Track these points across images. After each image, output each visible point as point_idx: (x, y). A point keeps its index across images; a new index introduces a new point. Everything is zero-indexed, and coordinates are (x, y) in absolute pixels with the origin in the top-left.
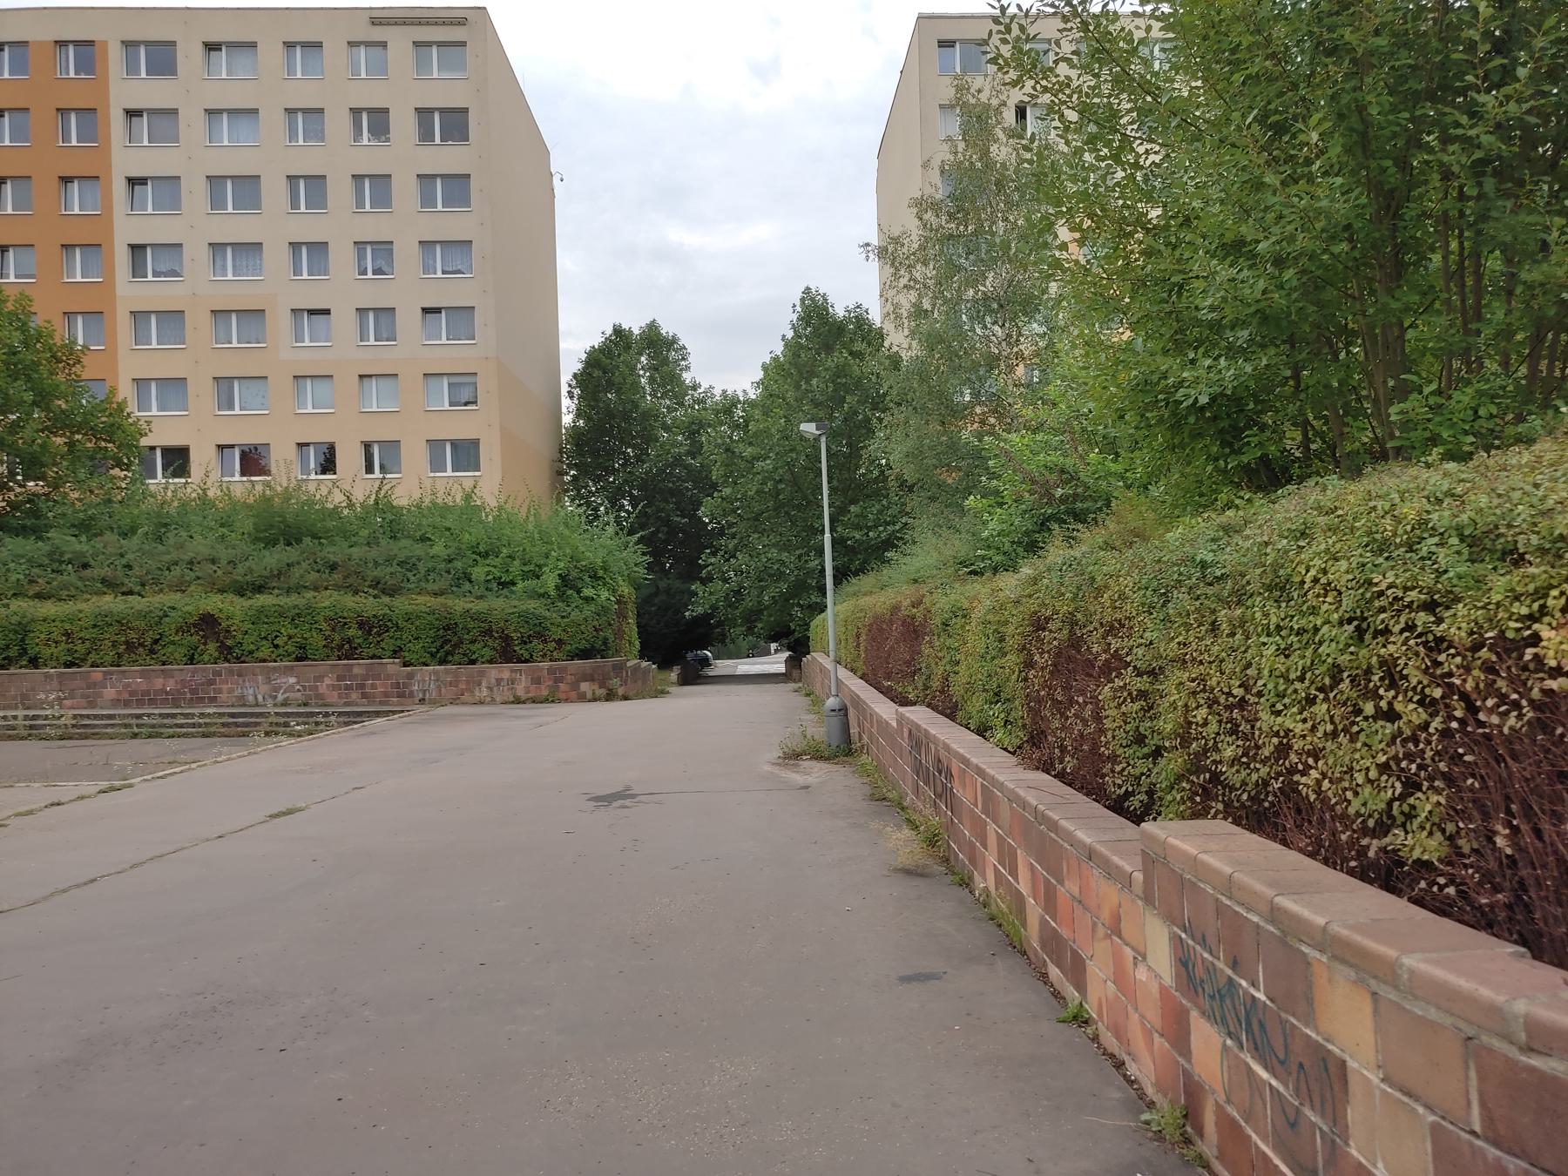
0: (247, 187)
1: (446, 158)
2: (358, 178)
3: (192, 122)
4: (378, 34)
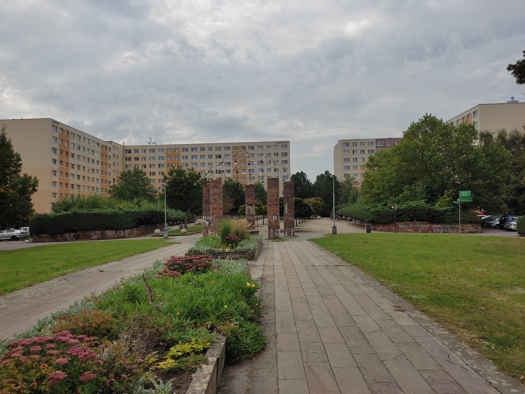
1: (285, 158)
4: (277, 144)
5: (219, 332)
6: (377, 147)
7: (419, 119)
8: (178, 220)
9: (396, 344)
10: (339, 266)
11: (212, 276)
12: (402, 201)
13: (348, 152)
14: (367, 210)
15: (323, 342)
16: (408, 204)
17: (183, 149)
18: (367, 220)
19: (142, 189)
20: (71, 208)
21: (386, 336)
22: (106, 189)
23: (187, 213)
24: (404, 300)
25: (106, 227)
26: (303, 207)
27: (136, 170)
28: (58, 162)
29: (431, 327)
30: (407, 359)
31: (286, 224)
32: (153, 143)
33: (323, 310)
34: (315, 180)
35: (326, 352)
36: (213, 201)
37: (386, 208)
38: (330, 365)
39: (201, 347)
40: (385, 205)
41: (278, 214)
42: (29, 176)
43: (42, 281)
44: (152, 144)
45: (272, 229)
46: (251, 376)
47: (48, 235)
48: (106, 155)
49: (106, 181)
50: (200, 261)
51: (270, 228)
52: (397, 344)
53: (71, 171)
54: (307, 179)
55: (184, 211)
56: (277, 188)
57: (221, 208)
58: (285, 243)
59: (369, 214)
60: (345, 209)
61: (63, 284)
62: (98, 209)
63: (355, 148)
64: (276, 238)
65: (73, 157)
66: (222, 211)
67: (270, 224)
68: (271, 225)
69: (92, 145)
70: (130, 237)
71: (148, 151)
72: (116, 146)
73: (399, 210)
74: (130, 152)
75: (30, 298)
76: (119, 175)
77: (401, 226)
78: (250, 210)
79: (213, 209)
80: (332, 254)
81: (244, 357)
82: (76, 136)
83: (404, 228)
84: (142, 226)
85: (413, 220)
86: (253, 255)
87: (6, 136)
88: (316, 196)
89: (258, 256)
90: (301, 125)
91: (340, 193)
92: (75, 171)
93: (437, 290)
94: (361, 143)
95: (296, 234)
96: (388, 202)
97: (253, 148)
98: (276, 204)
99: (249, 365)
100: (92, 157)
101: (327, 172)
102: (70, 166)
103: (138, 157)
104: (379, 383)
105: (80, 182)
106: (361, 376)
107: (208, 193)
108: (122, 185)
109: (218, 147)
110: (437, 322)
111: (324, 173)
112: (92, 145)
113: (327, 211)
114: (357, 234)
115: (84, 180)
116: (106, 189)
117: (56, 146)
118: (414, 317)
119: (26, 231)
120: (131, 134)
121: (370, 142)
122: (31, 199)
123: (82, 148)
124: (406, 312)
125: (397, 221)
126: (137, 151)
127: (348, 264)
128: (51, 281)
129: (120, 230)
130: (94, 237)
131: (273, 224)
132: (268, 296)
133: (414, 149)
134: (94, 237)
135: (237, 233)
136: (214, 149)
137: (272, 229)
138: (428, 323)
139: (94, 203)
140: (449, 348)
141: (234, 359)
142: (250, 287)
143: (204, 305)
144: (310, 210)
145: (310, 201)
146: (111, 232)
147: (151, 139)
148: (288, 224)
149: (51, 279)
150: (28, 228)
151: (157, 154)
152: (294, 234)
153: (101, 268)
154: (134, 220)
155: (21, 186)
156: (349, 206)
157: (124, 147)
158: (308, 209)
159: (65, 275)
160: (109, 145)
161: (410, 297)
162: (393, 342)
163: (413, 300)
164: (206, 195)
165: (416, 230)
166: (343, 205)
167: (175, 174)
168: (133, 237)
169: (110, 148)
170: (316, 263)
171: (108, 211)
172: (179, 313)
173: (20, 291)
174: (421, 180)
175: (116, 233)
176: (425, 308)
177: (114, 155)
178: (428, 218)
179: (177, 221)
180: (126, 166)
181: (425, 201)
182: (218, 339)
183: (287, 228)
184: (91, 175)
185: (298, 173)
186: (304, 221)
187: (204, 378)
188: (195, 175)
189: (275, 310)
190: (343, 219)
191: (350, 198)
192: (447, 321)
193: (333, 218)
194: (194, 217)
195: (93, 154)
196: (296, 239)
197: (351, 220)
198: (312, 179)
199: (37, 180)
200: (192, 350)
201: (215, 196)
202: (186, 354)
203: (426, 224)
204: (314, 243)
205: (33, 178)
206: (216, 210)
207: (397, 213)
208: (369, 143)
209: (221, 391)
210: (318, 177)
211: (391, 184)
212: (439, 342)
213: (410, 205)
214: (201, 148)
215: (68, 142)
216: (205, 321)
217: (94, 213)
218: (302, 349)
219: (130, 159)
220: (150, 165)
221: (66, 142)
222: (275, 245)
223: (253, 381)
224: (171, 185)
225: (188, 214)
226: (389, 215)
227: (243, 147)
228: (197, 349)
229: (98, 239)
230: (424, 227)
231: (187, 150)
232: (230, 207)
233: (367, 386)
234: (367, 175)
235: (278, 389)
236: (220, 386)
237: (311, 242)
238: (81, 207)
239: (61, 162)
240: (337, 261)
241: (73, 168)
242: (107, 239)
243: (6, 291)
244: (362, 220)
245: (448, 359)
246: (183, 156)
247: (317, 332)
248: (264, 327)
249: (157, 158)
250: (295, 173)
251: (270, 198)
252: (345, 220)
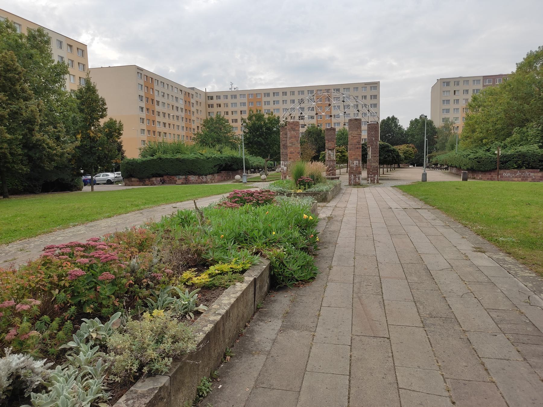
1: (374, 101)
5: (262, 256)
6: (484, 86)
7: (539, 47)
8: (259, 167)
9: (465, 282)
10: (420, 209)
11: (270, 208)
12: (509, 145)
14: (465, 157)
15: (381, 276)
16: (516, 149)
17: (265, 94)
18: (465, 168)
19: (225, 137)
20: (156, 153)
21: (456, 275)
22: (190, 137)
23: (266, 159)
24: (488, 242)
25: (189, 172)
26: (391, 152)
27: (218, 117)
28: (145, 109)
29: (514, 268)
30: (475, 297)
31: (370, 170)
32: (235, 89)
33: (389, 248)
34: (408, 126)
35: (381, 285)
36: (290, 145)
37: (488, 154)
38: (383, 297)
39: (240, 267)
40: (488, 150)
41: (360, 158)
42: (114, 120)
43: (120, 214)
44: (233, 90)
45: (352, 175)
46: (294, 301)
47: (137, 180)
48: (189, 102)
49: (190, 128)
50: (261, 195)
51: (350, 174)
52: (467, 283)
53: (158, 119)
54: (398, 124)
55: (264, 158)
56: (359, 130)
57: (298, 151)
58: (366, 189)
59: (468, 161)
60: (441, 157)
61: (137, 217)
62: (181, 155)
63: (456, 88)
64: (357, 185)
65: (158, 105)
66: (299, 155)
67: (351, 169)
68: (352, 171)
69: (175, 92)
70: (212, 182)
71: (229, 97)
72: (198, 93)
73: (504, 156)
74: (212, 98)
75: (106, 227)
76: (202, 123)
77: (506, 174)
78: (330, 155)
79: (291, 153)
80: (415, 199)
81: (290, 283)
82: (160, 82)
83: (509, 177)
84: (223, 172)
85: (521, 167)
86: (325, 196)
87: (91, 81)
88: (407, 143)
89: (332, 199)
90: (395, 64)
91: (436, 139)
92: (160, 119)
93: (532, 235)
94: (464, 81)
95: (380, 181)
96: (492, 147)
98: (358, 148)
99: (294, 292)
100: (176, 104)
102: (156, 113)
103: (220, 104)
104: (435, 317)
105: (166, 130)
106: (416, 310)
107: (285, 136)
108: (205, 132)
109: (301, 91)
110: (523, 264)
111: (418, 118)
112: (175, 92)
113: (421, 160)
114: (451, 182)
115: (170, 128)
116: (190, 137)
117: (142, 94)
118: (495, 258)
119: (119, 176)
120: (214, 80)
121: (476, 80)
122: (122, 146)
123: (166, 95)
124: (488, 254)
125: (500, 169)
126: (218, 97)
127: (430, 207)
128: (128, 215)
129: (202, 175)
130: (179, 182)
131: (354, 169)
132: (331, 233)
133: (529, 84)
134: (179, 182)
135: (312, 176)
136: (296, 93)
137: (352, 175)
138: (512, 264)
139: (178, 149)
140: (532, 290)
141: (280, 284)
142: (307, 219)
143: (252, 231)
145: (401, 149)
146: (194, 177)
147: (232, 84)
148: (371, 170)
149: (128, 213)
150: (120, 172)
151: (239, 100)
152: (378, 182)
153: (176, 205)
154: (215, 166)
155: (108, 130)
156: (446, 153)
157: (206, 93)
158: (396, 155)
159: (142, 209)
160: (191, 92)
161: (496, 240)
162: (462, 280)
163: (498, 242)
164: (283, 139)
165: (524, 179)
166: (439, 152)
167: (254, 118)
168: (215, 182)
169: (193, 95)
170: (393, 205)
171: (190, 156)
172: (223, 236)
173: (100, 221)
174: (536, 121)
175: (199, 178)
176: (512, 250)
177: (197, 102)
178: (540, 166)
179: (258, 168)
180: (209, 113)
181: (538, 146)
182: (261, 262)
183: (371, 175)
184: (177, 123)
185: (389, 118)
186: (393, 170)
187: (234, 294)
188: (275, 120)
189: (335, 246)
190: (438, 168)
191: (448, 145)
192: (536, 264)
194: (276, 165)
195: (177, 101)
196: (379, 185)
197: (447, 169)
198: (405, 124)
199: (121, 124)
200: (231, 270)
201: (292, 139)
202: (222, 273)
203: (537, 172)
204: (398, 189)
205: (118, 122)
206: (293, 155)
207: (502, 160)
208: (474, 81)
209: (260, 312)
210: (412, 122)
211: (497, 126)
212: (521, 284)
213: (519, 150)
214: (283, 92)
215: (152, 89)
216: (251, 246)
217: (177, 159)
218: (355, 281)
219: (212, 106)
220: (232, 112)
221: (151, 89)
222: (355, 190)
223: (295, 306)
224: (250, 130)
225: (268, 160)
226: (491, 162)
227: (327, 89)
228: (236, 269)
229: (182, 184)
230: (534, 176)
231: (268, 95)
232: (312, 154)
233: (420, 319)
234: (468, 118)
235: (319, 314)
236: (258, 307)
237: (395, 188)
238: (165, 152)
239: (148, 109)
240: (421, 204)
241: (159, 115)
242: (190, 183)
243: (87, 220)
244: (459, 168)
245: (528, 300)
246: (265, 102)
247: (376, 266)
248: (320, 259)
249: (239, 105)
250: (385, 118)
251: (351, 141)
252: (440, 168)
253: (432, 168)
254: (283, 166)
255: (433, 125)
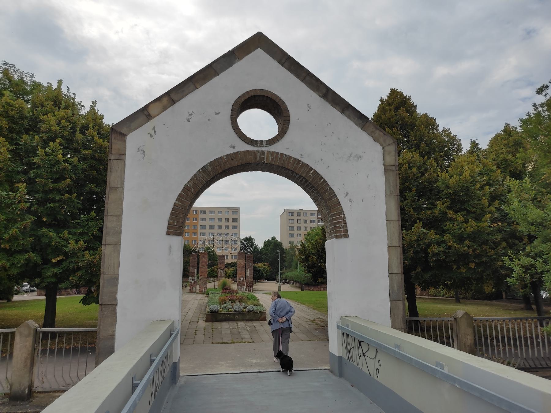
0: (213, 227)
1: (235, 224)
2: (218, 218)
3: (207, 220)
4: (228, 210)
13: (292, 221)
34: (263, 245)
36: (202, 267)
54: (254, 243)
60: (289, 274)
63: (298, 218)
79: (202, 272)
95: (254, 291)
97: (204, 212)
101: (273, 238)
113: (273, 276)
144: (262, 274)
148: (249, 284)
152: (253, 291)
156: (292, 271)
164: (192, 262)
185: (246, 238)
190: (287, 283)
191: (293, 264)
193: (279, 282)
197: (293, 283)
198: (260, 244)
208: (311, 213)
210: (265, 242)
244: (300, 283)
252: (289, 283)
253: (283, 282)
254: (191, 280)
255: (282, 246)
